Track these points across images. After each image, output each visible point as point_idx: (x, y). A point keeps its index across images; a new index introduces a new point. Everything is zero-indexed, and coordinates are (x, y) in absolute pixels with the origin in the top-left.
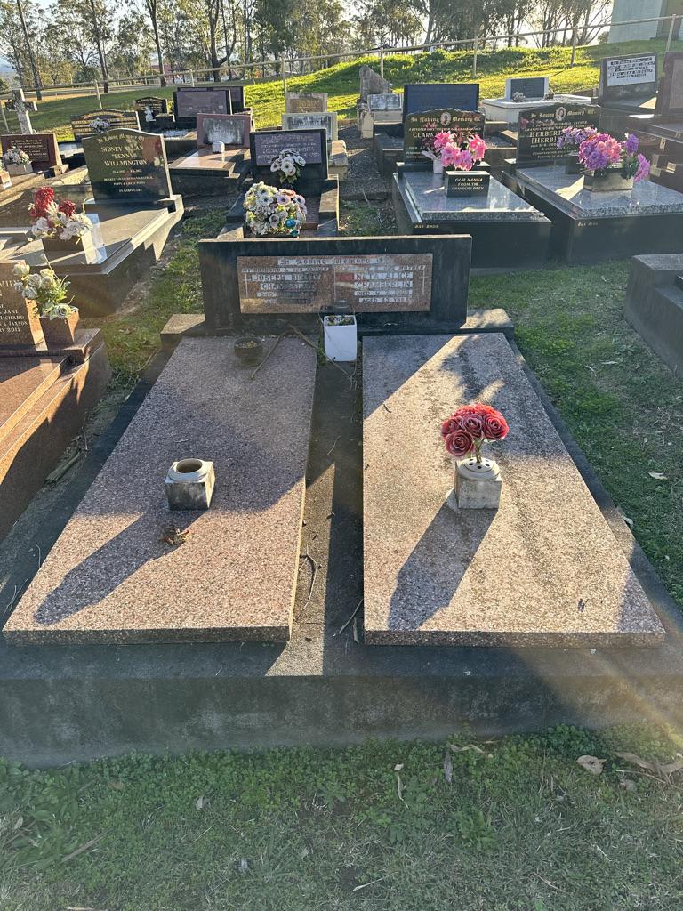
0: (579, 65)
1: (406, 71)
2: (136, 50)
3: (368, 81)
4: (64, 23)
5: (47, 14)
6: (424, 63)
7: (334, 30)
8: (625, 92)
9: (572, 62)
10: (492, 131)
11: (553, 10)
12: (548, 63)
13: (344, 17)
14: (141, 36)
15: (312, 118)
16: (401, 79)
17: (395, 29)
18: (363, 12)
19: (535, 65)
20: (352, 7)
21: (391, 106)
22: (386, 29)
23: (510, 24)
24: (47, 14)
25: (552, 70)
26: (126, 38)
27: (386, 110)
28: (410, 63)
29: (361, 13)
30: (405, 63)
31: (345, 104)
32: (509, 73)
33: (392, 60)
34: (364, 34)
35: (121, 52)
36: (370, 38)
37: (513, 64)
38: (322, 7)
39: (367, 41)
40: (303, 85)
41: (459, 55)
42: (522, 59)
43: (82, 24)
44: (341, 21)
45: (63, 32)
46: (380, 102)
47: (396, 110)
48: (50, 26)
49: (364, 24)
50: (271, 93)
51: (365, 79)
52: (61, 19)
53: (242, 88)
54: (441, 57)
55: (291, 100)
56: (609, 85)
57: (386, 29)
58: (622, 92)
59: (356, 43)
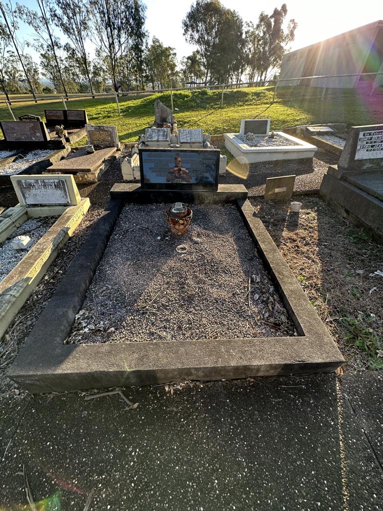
0: (276, 102)
1: (187, 101)
2: (100, 79)
3: (160, 110)
4: (71, 66)
5: (64, 62)
6: (197, 96)
7: (173, 74)
8: (370, 165)
10: (231, 199)
11: (253, 70)
12: (260, 100)
13: (177, 69)
14: (102, 73)
15: (43, 182)
16: (183, 106)
17: (196, 75)
18: (184, 67)
20: (180, 65)
21: (161, 138)
22: (193, 75)
23: (238, 75)
24: (64, 62)
25: (263, 106)
26: (96, 74)
27: (158, 141)
28: (189, 96)
29: (184, 68)
30: (187, 96)
31: (148, 123)
32: (241, 106)
33: (180, 94)
34: (185, 76)
35: (94, 79)
36: (187, 78)
37: (242, 99)
38: (169, 65)
39: (186, 79)
40: (132, 107)
41: (215, 92)
42: (246, 97)
43: (78, 67)
44: (176, 71)
45: (71, 70)
46: (154, 135)
47: (164, 141)
48: (66, 67)
49: (185, 72)
50: (114, 111)
51: (158, 108)
52: (70, 64)
53: (84, 111)
54: (204, 93)
55: (89, 131)
56: (356, 158)
57: (193, 75)
58: (368, 165)
59: (182, 79)
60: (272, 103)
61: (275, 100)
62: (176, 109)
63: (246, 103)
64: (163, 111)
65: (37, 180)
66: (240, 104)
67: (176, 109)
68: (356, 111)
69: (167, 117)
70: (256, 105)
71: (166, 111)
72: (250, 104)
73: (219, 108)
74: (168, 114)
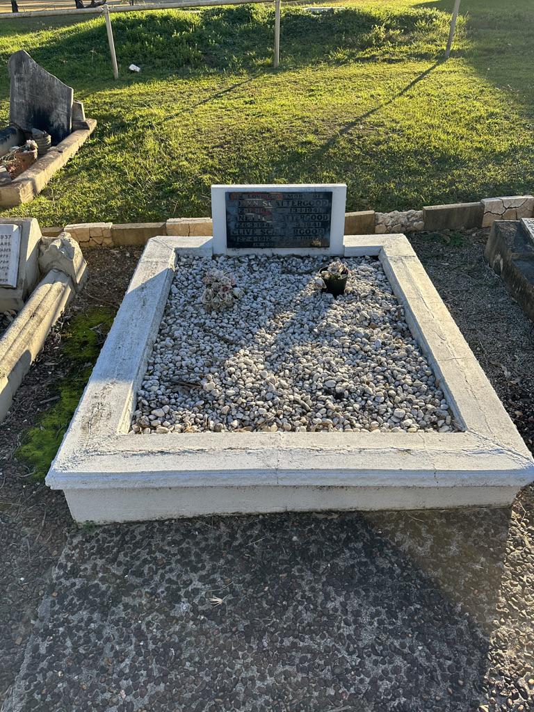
1: (178, 42)
3: (26, 85)
9: (448, 46)
19: (388, 47)
30: (182, 25)
32: (339, 63)
33: (166, 19)
51: (20, 80)
60: (442, 57)
61: (454, 47)
62: (133, 67)
63: (360, 54)
64: (37, 87)
65: (443, 398)
66: (340, 56)
67: (133, 67)
68: (90, 299)
69: (51, 110)
70: (390, 61)
71: (51, 87)
72: (373, 59)
73: (271, 69)
74: (57, 101)
